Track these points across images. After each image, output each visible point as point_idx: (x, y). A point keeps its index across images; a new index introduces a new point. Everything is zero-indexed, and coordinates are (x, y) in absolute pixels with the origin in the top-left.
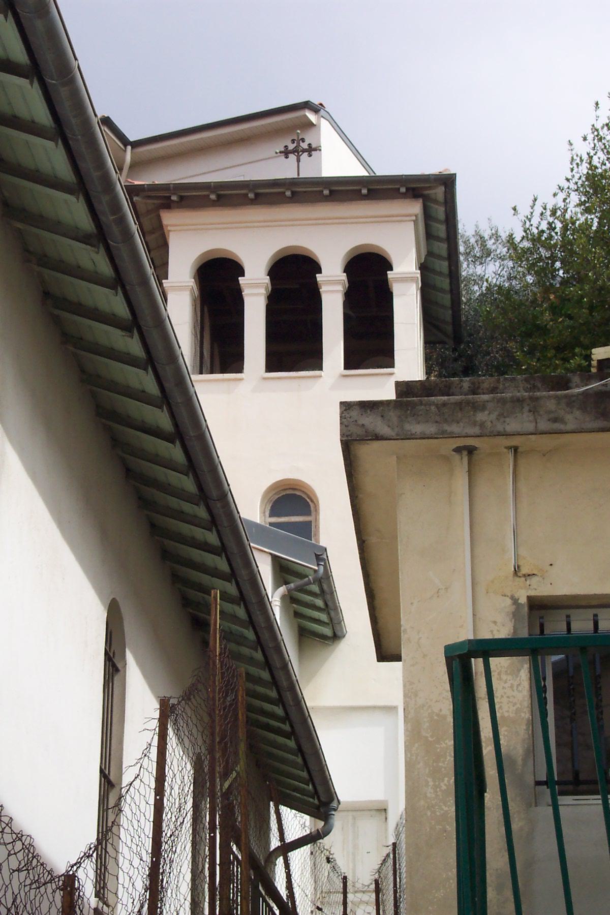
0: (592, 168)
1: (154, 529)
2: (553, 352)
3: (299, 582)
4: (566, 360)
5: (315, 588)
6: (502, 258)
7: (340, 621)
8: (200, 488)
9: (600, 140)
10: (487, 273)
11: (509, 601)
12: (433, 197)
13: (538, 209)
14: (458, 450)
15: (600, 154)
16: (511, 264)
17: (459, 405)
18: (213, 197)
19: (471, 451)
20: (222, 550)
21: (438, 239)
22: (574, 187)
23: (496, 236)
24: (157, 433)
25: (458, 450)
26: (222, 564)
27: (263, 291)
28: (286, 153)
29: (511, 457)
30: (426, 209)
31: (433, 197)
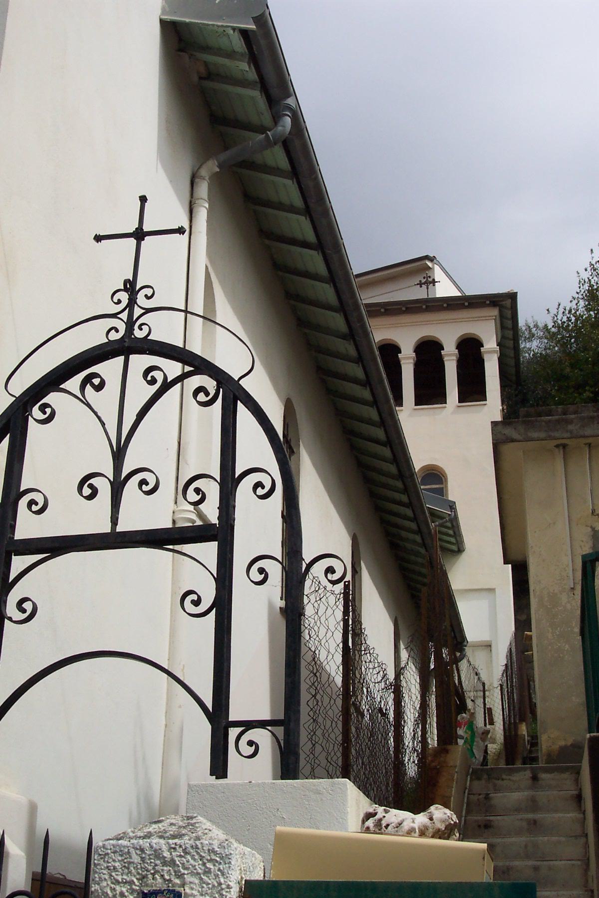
0: (591, 286)
1: (372, 495)
2: (572, 390)
3: (441, 521)
4: (580, 394)
5: (449, 524)
6: (541, 338)
7: (462, 542)
8: (399, 471)
9: (595, 270)
10: (533, 347)
11: (590, 529)
12: (504, 305)
13: (561, 310)
14: (557, 446)
15: (595, 278)
16: (546, 341)
17: (558, 421)
18: (382, 310)
19: (564, 446)
20: (409, 505)
21: (507, 328)
22: (581, 297)
23: (536, 326)
24: (377, 442)
25: (557, 446)
26: (409, 512)
27: (412, 361)
28: (421, 284)
29: (587, 449)
30: (500, 312)
31: (504, 305)
